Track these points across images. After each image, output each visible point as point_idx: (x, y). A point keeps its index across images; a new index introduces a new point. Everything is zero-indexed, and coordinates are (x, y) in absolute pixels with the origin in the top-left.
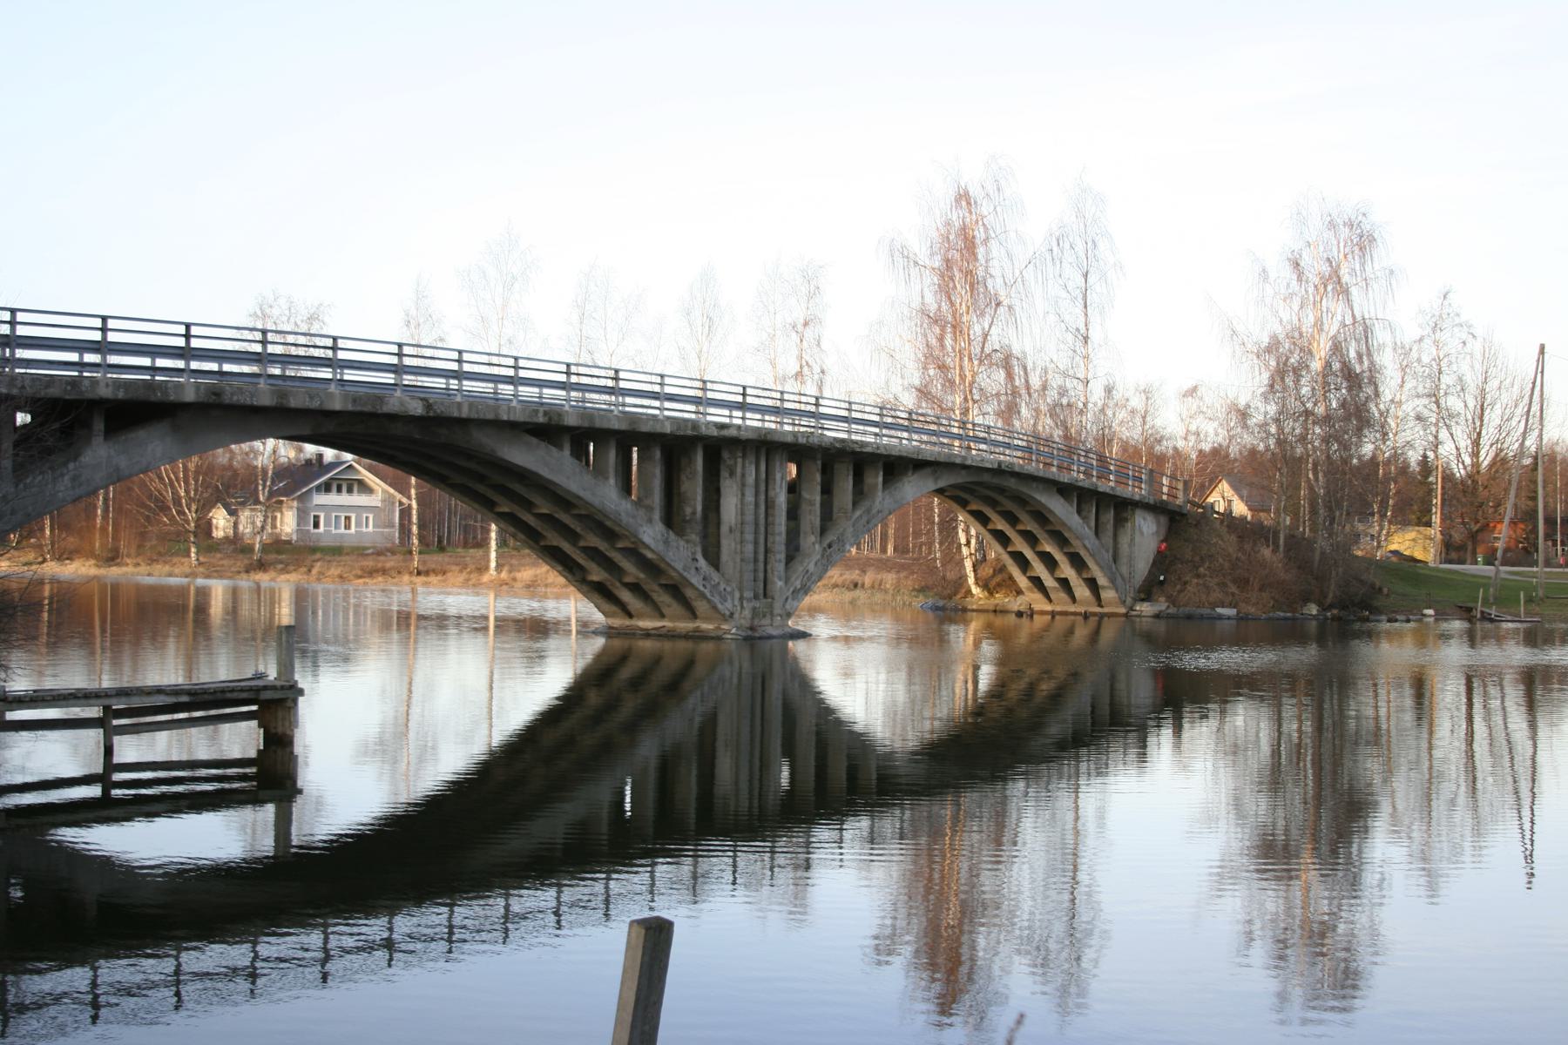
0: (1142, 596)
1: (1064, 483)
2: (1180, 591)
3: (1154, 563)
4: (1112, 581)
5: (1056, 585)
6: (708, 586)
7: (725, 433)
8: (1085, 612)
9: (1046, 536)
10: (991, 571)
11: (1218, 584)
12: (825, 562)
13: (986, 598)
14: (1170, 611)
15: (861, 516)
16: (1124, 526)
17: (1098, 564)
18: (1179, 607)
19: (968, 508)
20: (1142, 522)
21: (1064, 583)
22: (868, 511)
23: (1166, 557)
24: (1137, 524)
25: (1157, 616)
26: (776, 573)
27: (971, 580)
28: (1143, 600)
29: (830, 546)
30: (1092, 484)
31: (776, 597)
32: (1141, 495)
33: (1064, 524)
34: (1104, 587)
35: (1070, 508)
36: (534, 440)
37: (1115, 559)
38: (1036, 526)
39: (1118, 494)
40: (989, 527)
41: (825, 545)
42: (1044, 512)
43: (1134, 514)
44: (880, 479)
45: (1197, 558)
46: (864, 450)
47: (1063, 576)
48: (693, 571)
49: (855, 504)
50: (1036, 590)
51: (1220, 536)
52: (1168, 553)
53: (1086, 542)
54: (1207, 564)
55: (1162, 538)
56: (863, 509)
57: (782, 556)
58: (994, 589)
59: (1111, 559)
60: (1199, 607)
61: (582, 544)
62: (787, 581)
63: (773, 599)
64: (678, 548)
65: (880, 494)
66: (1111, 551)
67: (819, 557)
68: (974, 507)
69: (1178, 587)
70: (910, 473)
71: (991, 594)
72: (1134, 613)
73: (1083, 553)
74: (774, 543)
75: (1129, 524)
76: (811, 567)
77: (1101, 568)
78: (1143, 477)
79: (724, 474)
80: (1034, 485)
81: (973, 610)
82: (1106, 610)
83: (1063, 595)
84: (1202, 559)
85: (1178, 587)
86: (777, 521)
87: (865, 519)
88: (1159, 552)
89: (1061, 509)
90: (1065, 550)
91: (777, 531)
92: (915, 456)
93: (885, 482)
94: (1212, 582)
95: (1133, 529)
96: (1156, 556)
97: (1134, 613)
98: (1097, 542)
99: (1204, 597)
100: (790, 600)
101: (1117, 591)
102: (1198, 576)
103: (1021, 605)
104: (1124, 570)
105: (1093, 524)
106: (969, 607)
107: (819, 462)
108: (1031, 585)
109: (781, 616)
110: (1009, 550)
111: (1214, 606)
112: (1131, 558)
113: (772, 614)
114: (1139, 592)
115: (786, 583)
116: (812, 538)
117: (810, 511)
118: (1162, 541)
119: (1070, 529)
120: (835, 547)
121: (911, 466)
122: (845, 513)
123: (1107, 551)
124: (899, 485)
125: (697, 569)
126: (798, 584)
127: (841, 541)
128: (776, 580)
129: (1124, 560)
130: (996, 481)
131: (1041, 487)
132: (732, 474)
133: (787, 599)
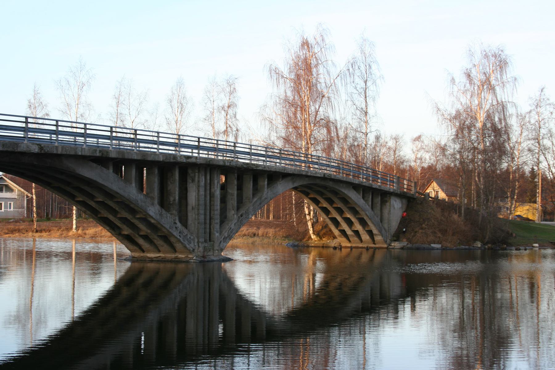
0: (395, 239)
4: (380, 231)
6: (182, 236)
7: (189, 160)
8: (367, 247)
9: (347, 209)
10: (321, 227)
13: (318, 240)
14: (409, 246)
15: (257, 201)
16: (385, 205)
17: (373, 223)
20: (394, 203)
21: (357, 233)
22: (260, 198)
24: (392, 204)
25: (402, 248)
26: (215, 229)
27: (311, 232)
28: (395, 241)
29: (242, 216)
31: (215, 241)
32: (393, 189)
33: (356, 204)
34: (376, 235)
35: (359, 196)
36: (95, 165)
38: (343, 205)
39: (382, 189)
40: (319, 206)
43: (390, 198)
44: (266, 183)
45: (421, 220)
46: (258, 169)
47: (356, 229)
48: (174, 229)
49: (254, 195)
50: (343, 236)
53: (367, 213)
54: (426, 223)
55: (404, 210)
56: (258, 197)
59: (379, 220)
60: (422, 244)
63: (214, 242)
64: (167, 217)
65: (266, 190)
66: (379, 217)
69: (412, 234)
70: (280, 180)
71: (321, 238)
72: (391, 247)
73: (365, 218)
74: (214, 214)
75: (388, 204)
77: (375, 225)
78: (395, 180)
79: (189, 181)
80: (341, 185)
81: (312, 247)
82: (377, 246)
83: (356, 239)
84: (424, 220)
85: (412, 234)
88: (403, 217)
89: (354, 196)
90: (357, 217)
91: (215, 209)
92: (283, 171)
93: (268, 184)
95: (390, 206)
97: (391, 247)
98: (372, 213)
100: (222, 243)
102: (422, 229)
103: (335, 244)
104: (386, 226)
105: (370, 203)
106: (310, 245)
107: (236, 175)
109: (218, 250)
111: (430, 243)
113: (213, 250)
114: (393, 237)
115: (220, 234)
116: (233, 212)
117: (232, 198)
118: (404, 212)
119: (359, 206)
120: (244, 216)
121: (281, 176)
123: (377, 217)
125: (176, 228)
126: (226, 235)
127: (247, 213)
128: (215, 232)
130: (323, 183)
132: (193, 181)
133: (221, 242)
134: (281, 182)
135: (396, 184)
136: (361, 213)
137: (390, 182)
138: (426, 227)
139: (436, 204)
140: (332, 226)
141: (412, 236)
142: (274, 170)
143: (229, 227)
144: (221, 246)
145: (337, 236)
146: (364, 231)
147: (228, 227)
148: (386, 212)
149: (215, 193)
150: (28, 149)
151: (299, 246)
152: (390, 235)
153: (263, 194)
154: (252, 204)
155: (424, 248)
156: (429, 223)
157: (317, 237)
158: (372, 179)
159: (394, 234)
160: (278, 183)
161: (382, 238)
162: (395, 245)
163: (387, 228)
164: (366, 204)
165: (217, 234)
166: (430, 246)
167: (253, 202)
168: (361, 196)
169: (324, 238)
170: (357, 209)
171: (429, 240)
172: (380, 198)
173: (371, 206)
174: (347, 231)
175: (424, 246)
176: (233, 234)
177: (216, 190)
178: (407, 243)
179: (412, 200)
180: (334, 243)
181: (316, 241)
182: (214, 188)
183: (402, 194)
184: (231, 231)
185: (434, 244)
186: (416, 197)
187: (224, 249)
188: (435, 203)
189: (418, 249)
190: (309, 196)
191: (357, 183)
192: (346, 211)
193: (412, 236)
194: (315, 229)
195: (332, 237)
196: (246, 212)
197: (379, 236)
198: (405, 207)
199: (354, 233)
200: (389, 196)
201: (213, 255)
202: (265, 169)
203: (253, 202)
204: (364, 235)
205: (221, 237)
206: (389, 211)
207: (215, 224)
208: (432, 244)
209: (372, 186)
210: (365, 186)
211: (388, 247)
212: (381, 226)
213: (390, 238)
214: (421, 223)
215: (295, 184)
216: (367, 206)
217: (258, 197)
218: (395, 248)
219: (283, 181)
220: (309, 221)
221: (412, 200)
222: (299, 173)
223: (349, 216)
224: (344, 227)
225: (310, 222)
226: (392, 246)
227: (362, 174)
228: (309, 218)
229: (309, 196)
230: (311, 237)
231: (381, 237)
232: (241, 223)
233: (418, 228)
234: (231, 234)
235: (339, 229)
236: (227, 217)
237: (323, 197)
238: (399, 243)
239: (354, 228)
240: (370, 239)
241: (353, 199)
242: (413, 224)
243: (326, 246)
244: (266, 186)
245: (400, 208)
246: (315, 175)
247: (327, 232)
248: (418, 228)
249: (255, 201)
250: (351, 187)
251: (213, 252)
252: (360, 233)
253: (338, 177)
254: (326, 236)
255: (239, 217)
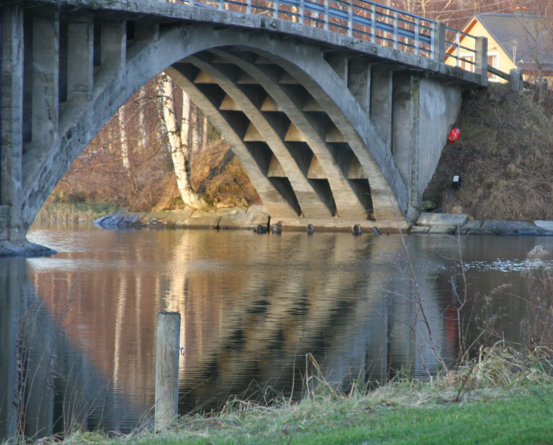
0: (429, 205)
1: (336, 46)
2: (485, 197)
3: (443, 158)
4: (390, 182)
5: (309, 189)
8: (356, 228)
9: (304, 120)
10: (207, 170)
11: (536, 188)
12: (63, 156)
13: (204, 209)
14: (471, 225)
15: (103, 94)
16: (404, 106)
17: (373, 158)
18: (483, 220)
19: (197, 81)
20: (428, 99)
22: (111, 88)
23: (460, 149)
24: (421, 102)
25: (453, 232)
26: (13, 171)
27: (182, 183)
28: (429, 210)
29: (69, 136)
30: (372, 47)
31: (14, 204)
32: (429, 61)
33: (332, 103)
34: (378, 193)
35: (340, 81)
37: (394, 148)
38: (292, 106)
39: (402, 60)
40: (222, 107)
41: (64, 134)
42: (306, 86)
43: (418, 87)
44: (124, 45)
45: (504, 151)
46: (113, 8)
47: (320, 177)
49: (96, 75)
50: (279, 197)
51: (536, 120)
52: (463, 143)
53: (359, 129)
54: (519, 159)
55: (452, 122)
56: (105, 85)
57: (18, 149)
58: (215, 196)
59: (389, 151)
60: (509, 219)
61: (225, 106)
62: (24, 180)
63: (10, 205)
65: (123, 64)
66: (389, 141)
67: (57, 149)
68: (206, 79)
69: (480, 191)
70: (156, 37)
71: (210, 203)
72: (419, 229)
73: (353, 144)
74: (10, 131)
75: (412, 103)
76: (50, 163)
77: (378, 165)
78: (433, 35)
80: (298, 49)
81: (185, 227)
82: (379, 225)
83: (319, 204)
84: (512, 152)
85: (480, 191)
86: (14, 103)
87: (105, 102)
88: (449, 142)
90: (328, 140)
91: (14, 117)
92: (168, 14)
93: (128, 47)
94: (528, 185)
95: (417, 109)
96: (445, 147)
97: (419, 229)
98: (372, 128)
99: (516, 206)
100: (27, 207)
101: (396, 197)
102: (507, 176)
103: (254, 219)
104: (405, 167)
105: (367, 102)
106: (179, 222)
107: (57, 24)
108: (273, 189)
109: (19, 227)
110: (246, 139)
111: (531, 218)
112: (414, 151)
113: (9, 226)
114: (424, 199)
115: (23, 184)
117: (46, 88)
118: (454, 127)
119: (339, 110)
120: (75, 136)
121: (157, 27)
122: (85, 91)
123: (385, 141)
124: (144, 52)
126: (35, 186)
128: (14, 179)
129: (405, 154)
130: (253, 44)
131: (305, 51)
133: (23, 205)
134: (157, 44)
135: (435, 45)
136: (341, 128)
137: (420, 39)
138: (519, 171)
139: (544, 104)
140: (252, 167)
141: (480, 198)
142: (149, 12)
143: (42, 166)
144: (25, 216)
145: (261, 196)
146: (346, 182)
147: (39, 165)
148: (407, 126)
149: (14, 74)
150: (431, 63)
151: (145, 226)
152: (416, 195)
153: (117, 78)
154: (92, 103)
155: (516, 231)
156: (527, 161)
157: (199, 199)
158: (353, 24)
159: (424, 193)
160: (151, 45)
161: (395, 203)
162: (431, 223)
163: (408, 176)
164: (358, 105)
165: (18, 185)
166: (531, 227)
167: (95, 99)
168: (344, 83)
169: (219, 201)
170: (333, 118)
171: (527, 209)
172: (391, 86)
173: (368, 110)
174: (293, 182)
175: (516, 227)
176: (51, 184)
177: (16, 66)
178: (466, 216)
179: (473, 92)
180: (251, 217)
181: (195, 209)
182: (11, 60)
183: (451, 75)
184: (46, 177)
185: (544, 219)
186: (486, 85)
187: (31, 224)
188: (541, 100)
189: (498, 234)
190: (198, 81)
191: (340, 43)
192: (299, 125)
193: (480, 198)
194: (191, 178)
195: (244, 200)
196: (78, 124)
197: (386, 198)
198: (455, 112)
199: (315, 188)
200: (416, 82)
201: (9, 239)
202: (129, 9)
203: (95, 99)
204: (344, 194)
205: (25, 193)
206: (414, 124)
207: (13, 156)
208: (538, 219)
209: (376, 52)
210: (357, 53)
211: (410, 228)
212: (393, 166)
213: (415, 203)
214: (504, 159)
215: (189, 47)
216: (360, 110)
217: (105, 85)
218: (432, 230)
219: (162, 40)
220: (175, 151)
221: (473, 92)
222: (204, 19)
223: (303, 138)
224: (285, 169)
225: (178, 153)
226: (421, 225)
227: (327, 11)
228: (178, 145)
229: (198, 81)
230: (180, 198)
231: (392, 198)
232: (67, 154)
233: (496, 175)
234: (46, 186)
235: (270, 175)
236: (33, 139)
237: (240, 82)
238: (443, 218)
239: (315, 174)
240: (360, 204)
241: (324, 88)
242: (480, 161)
243: (228, 224)
244: (123, 55)
245: (441, 116)
246: (241, 24)
247: (228, 184)
248: (496, 175)
249: (100, 97)
250: (322, 55)
251: (9, 233)
252: (332, 188)
253: (294, 29)
254: (225, 198)
255: (63, 138)
